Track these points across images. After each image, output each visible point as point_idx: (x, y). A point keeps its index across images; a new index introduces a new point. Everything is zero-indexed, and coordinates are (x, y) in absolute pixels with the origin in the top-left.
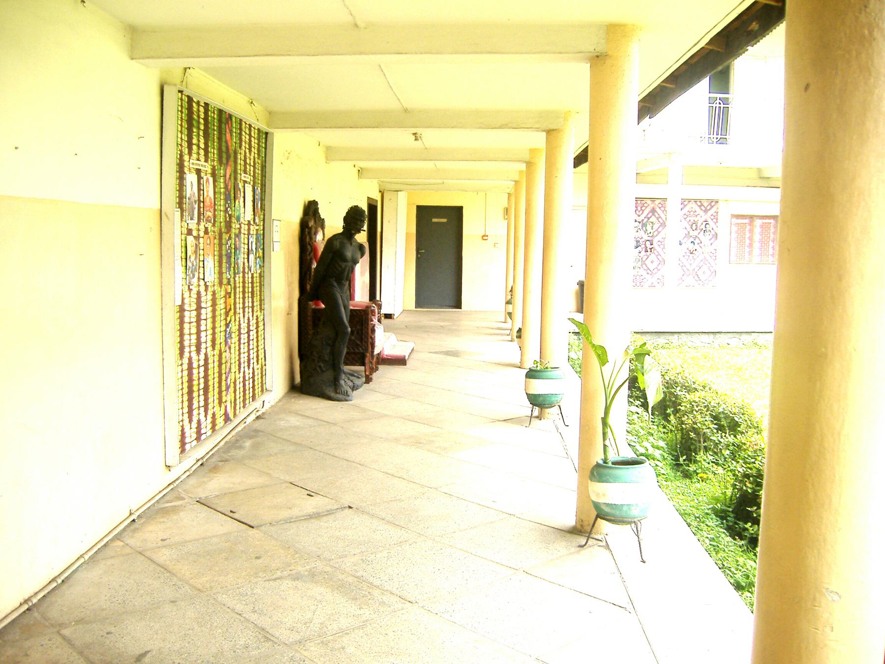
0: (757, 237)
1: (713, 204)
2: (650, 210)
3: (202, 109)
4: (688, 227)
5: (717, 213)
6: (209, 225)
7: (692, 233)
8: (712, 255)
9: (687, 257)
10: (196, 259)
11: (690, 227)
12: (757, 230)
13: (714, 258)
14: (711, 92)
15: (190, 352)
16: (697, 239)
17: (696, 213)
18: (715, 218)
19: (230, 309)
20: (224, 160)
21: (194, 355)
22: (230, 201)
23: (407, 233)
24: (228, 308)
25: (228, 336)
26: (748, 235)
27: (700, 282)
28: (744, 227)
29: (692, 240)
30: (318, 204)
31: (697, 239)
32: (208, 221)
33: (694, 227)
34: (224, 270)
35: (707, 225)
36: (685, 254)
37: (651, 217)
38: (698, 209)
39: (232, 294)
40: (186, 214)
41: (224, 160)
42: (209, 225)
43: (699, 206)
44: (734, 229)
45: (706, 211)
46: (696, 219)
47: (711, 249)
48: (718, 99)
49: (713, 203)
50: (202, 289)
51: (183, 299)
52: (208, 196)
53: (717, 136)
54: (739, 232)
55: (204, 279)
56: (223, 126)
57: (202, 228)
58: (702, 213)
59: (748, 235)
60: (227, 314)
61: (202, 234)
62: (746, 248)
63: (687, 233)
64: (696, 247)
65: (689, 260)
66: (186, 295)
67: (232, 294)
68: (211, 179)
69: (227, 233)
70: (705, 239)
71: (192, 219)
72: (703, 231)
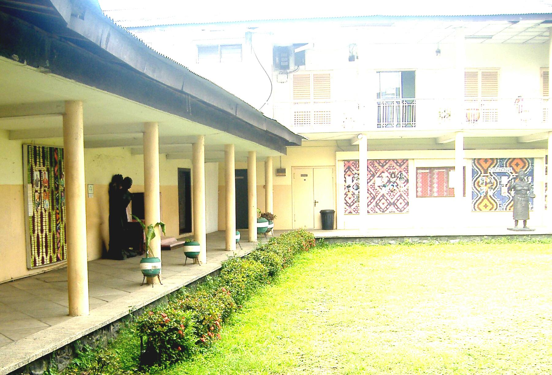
0: (435, 181)
1: (405, 161)
2: (347, 167)
3: (41, 149)
4: (389, 176)
5: (408, 167)
6: (46, 189)
7: (391, 180)
8: (405, 192)
9: (389, 194)
10: (39, 200)
11: (390, 176)
12: (435, 176)
13: (407, 194)
14: (403, 97)
15: (38, 232)
16: (395, 183)
17: (394, 168)
18: (407, 170)
19: (59, 219)
20: (54, 165)
21: (40, 234)
22: (58, 179)
23: (219, 186)
24: (57, 218)
25: (58, 229)
26: (429, 179)
27: (398, 209)
28: (427, 175)
29: (392, 184)
30: (122, 176)
31: (395, 183)
32: (45, 187)
33: (393, 176)
34: (55, 204)
35: (402, 175)
36: (388, 193)
37: (348, 171)
38: (395, 165)
39: (60, 214)
40: (34, 186)
41: (54, 165)
42: (46, 189)
43: (395, 163)
44: (420, 176)
45: (400, 166)
46: (394, 171)
47: (405, 188)
48: (404, 101)
49: (405, 161)
50: (43, 211)
51: (34, 214)
52: (45, 178)
53: (386, 123)
54: (423, 178)
55: (44, 208)
56: (53, 153)
57: (42, 189)
58: (398, 167)
59: (429, 179)
60: (57, 220)
61: (42, 192)
62: (428, 187)
63: (389, 179)
64: (395, 188)
65: (391, 196)
66: (36, 213)
67: (60, 214)
68: (47, 173)
69: (56, 191)
70: (400, 183)
71: (37, 187)
72: (399, 178)
